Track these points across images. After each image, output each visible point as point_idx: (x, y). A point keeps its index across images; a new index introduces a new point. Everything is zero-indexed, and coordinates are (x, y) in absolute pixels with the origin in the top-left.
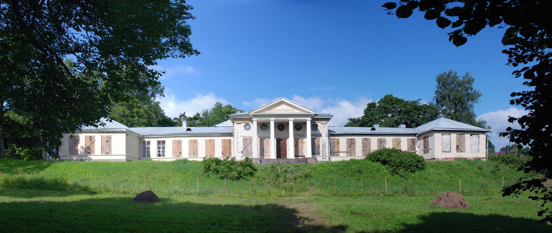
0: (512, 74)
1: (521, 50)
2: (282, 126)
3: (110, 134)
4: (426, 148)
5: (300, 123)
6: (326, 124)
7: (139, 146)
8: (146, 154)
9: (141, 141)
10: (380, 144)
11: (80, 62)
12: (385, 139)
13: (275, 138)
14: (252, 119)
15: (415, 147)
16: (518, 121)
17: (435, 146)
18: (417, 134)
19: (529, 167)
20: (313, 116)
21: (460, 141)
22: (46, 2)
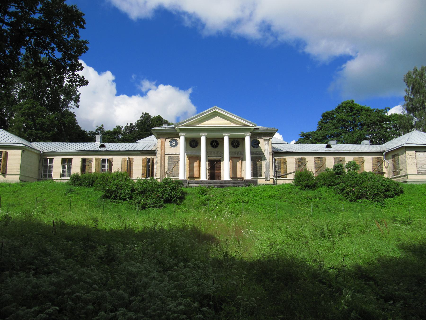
0: (81, 93)
1: (11, 71)
2: (216, 142)
3: (131, 157)
4: (396, 169)
5: (237, 138)
6: (269, 140)
8: (48, 173)
9: (42, 159)
12: (344, 158)
13: (206, 161)
14: (179, 134)
15: (383, 167)
17: (407, 166)
18: (384, 152)
20: (252, 130)
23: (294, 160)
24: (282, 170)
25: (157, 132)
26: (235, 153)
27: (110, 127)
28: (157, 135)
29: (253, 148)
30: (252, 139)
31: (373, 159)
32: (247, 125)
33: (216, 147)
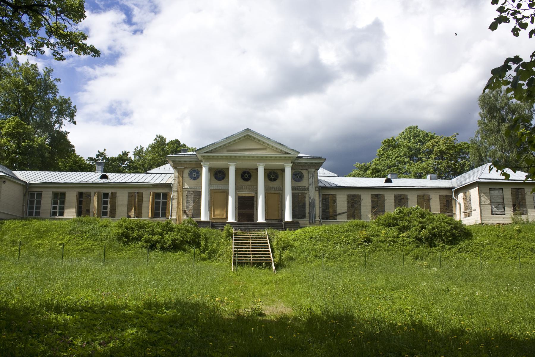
7: (24, 200)
9: (27, 192)
10: (399, 203)
11: (41, 135)
16: (384, 211)
18: (454, 189)
19: (89, 159)
21: (517, 198)
22: (534, 331)
23: (346, 197)
24: (331, 210)
25: (173, 160)
26: (272, 188)
27: (113, 153)
28: (174, 163)
29: (295, 182)
30: (294, 171)
31: (441, 197)
32: (288, 153)
33: (248, 180)
